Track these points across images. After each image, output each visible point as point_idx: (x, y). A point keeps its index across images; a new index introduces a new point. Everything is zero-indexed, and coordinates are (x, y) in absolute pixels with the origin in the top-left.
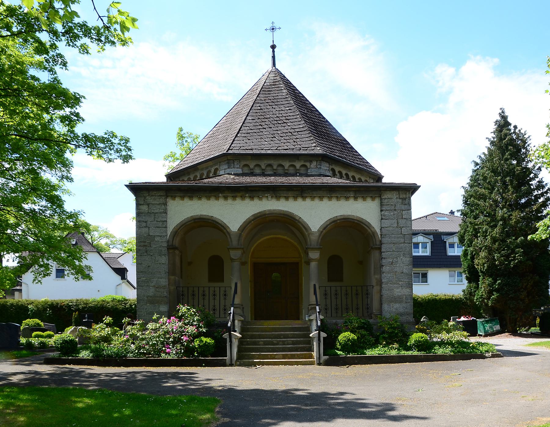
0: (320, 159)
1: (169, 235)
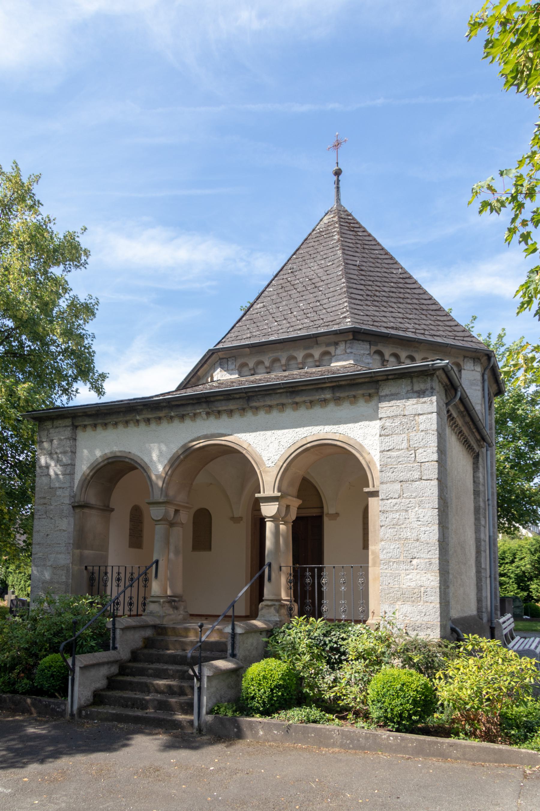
0: (351, 337)
1: (76, 486)
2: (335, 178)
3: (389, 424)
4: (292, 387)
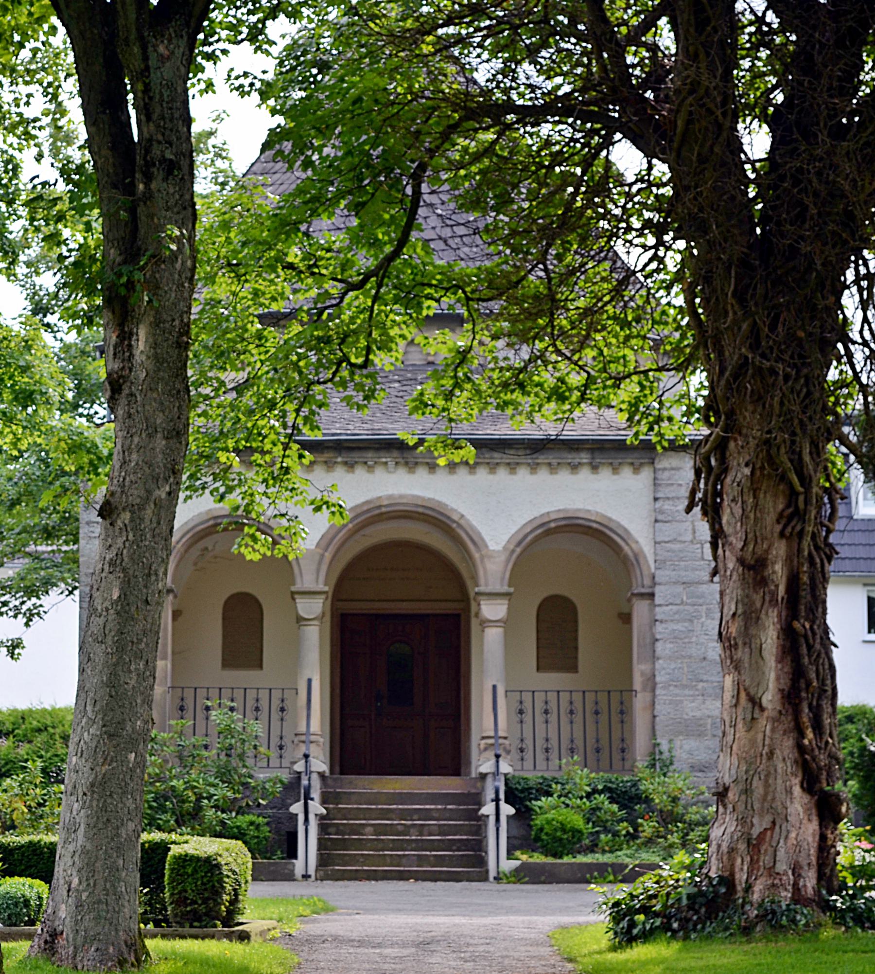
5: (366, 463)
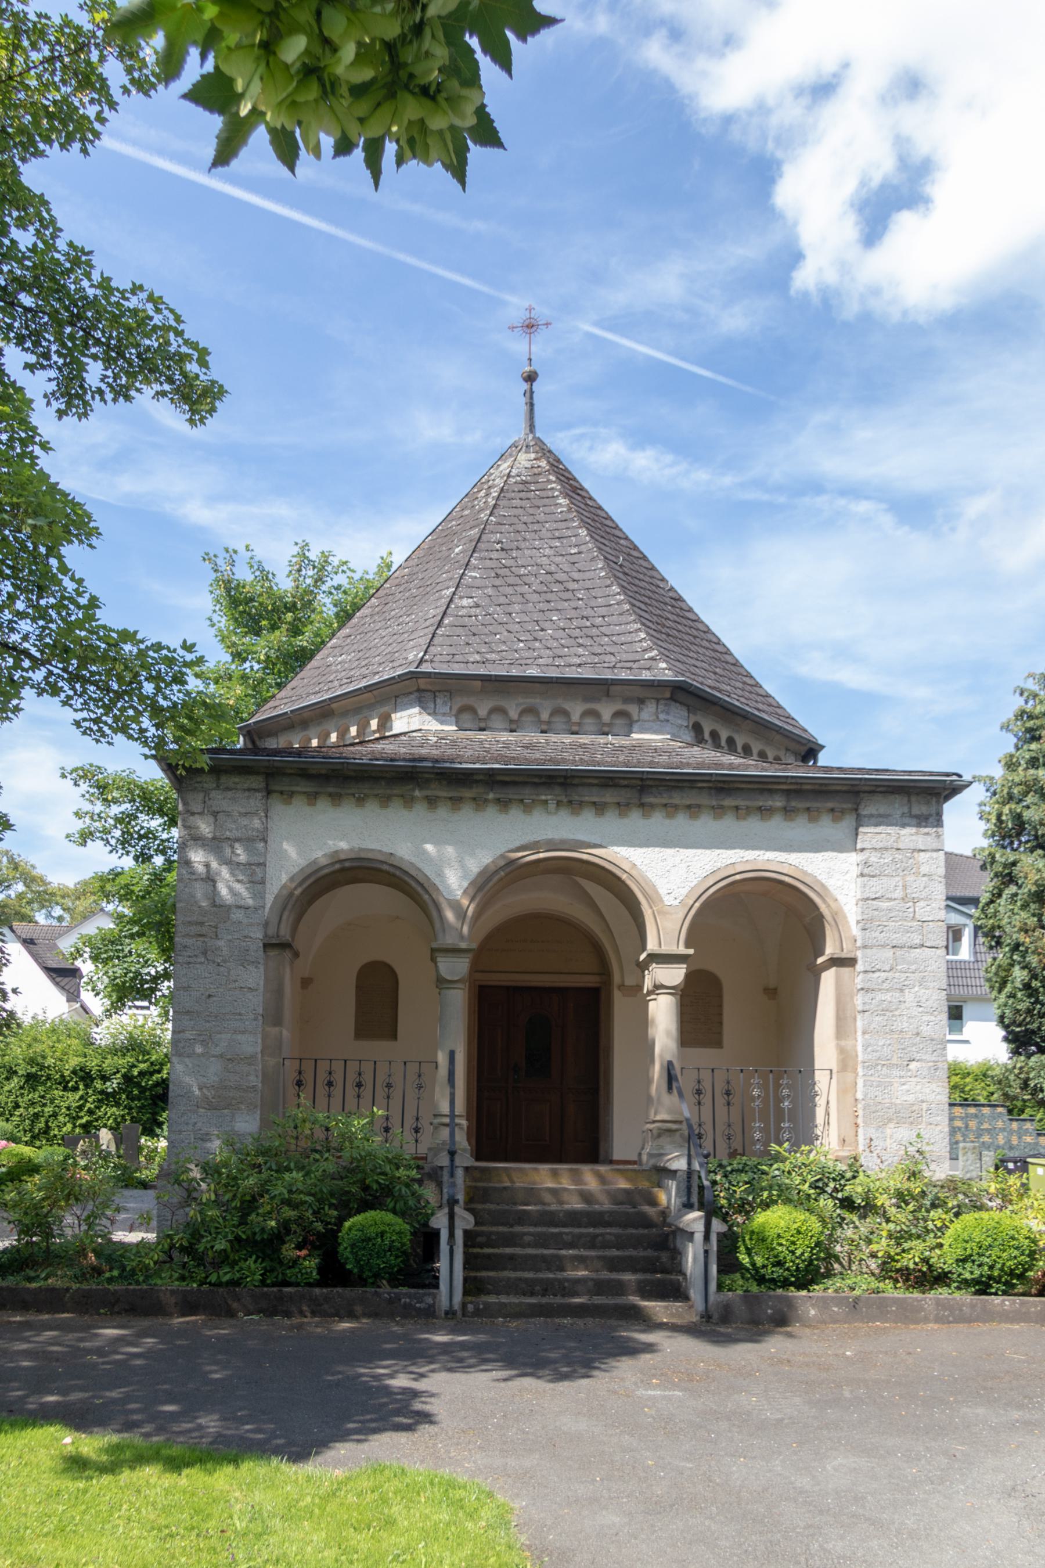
0: (668, 695)
1: (268, 906)
2: (525, 386)
3: (876, 860)
4: (724, 782)
5: (522, 801)
